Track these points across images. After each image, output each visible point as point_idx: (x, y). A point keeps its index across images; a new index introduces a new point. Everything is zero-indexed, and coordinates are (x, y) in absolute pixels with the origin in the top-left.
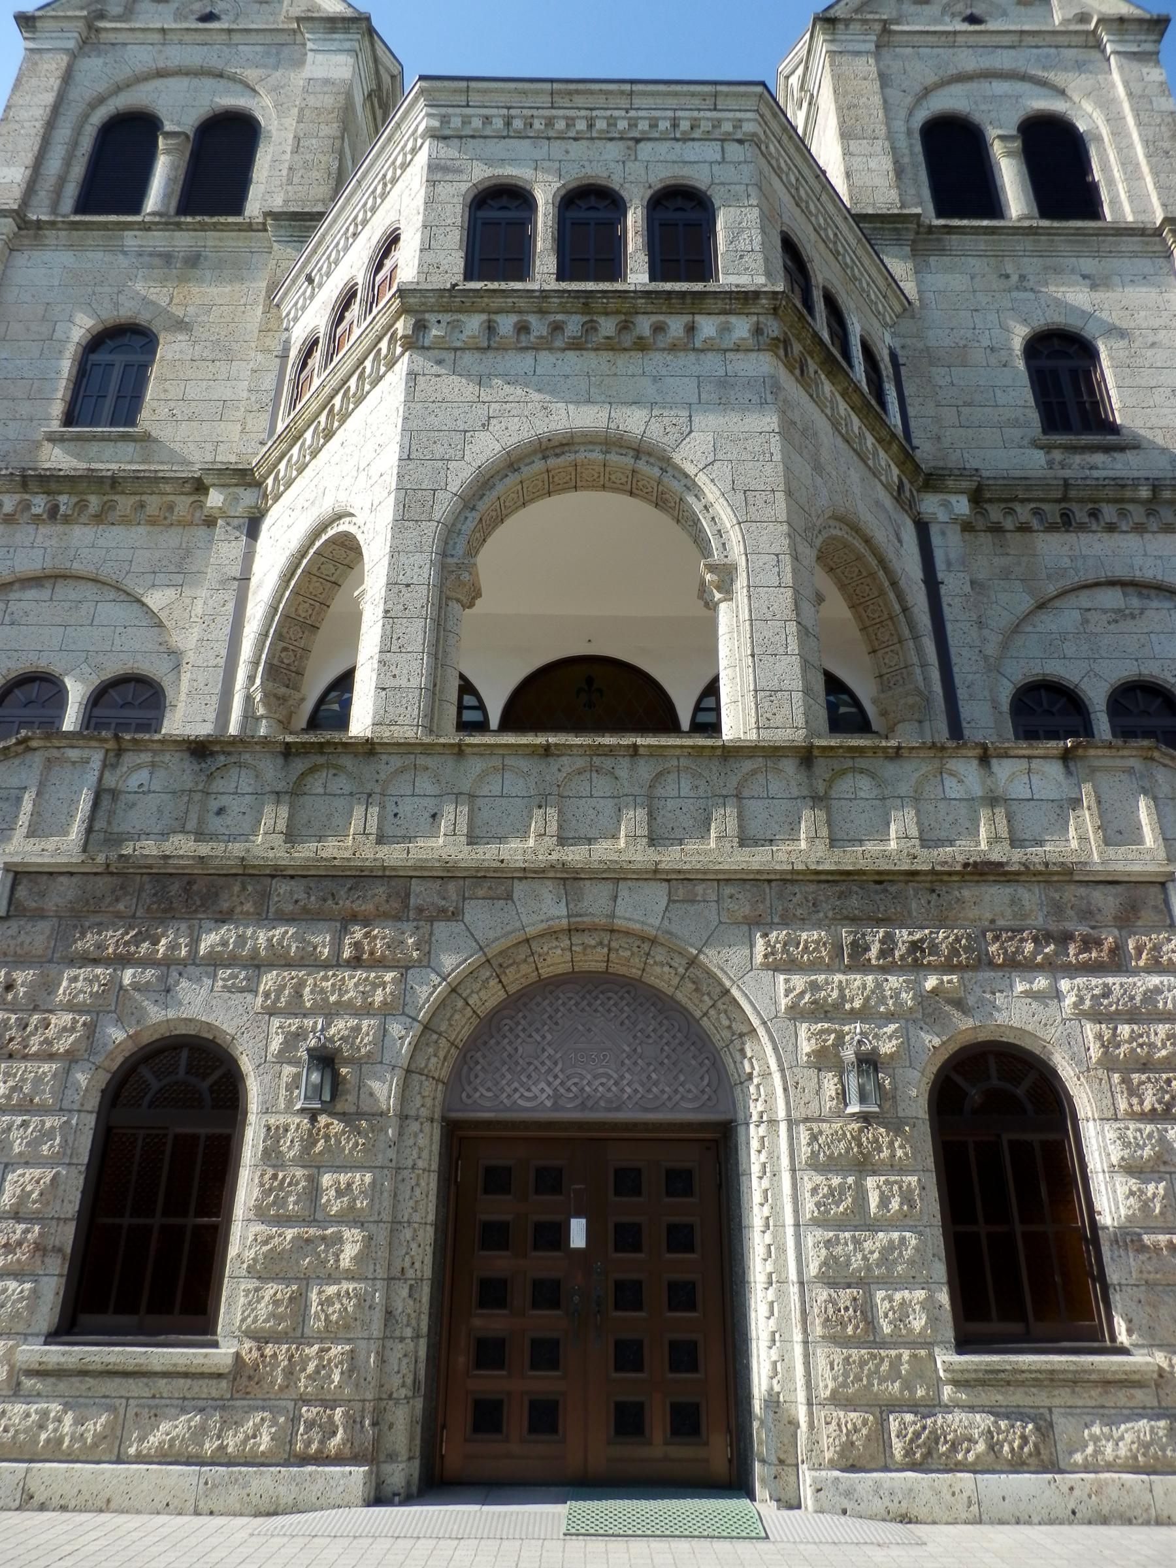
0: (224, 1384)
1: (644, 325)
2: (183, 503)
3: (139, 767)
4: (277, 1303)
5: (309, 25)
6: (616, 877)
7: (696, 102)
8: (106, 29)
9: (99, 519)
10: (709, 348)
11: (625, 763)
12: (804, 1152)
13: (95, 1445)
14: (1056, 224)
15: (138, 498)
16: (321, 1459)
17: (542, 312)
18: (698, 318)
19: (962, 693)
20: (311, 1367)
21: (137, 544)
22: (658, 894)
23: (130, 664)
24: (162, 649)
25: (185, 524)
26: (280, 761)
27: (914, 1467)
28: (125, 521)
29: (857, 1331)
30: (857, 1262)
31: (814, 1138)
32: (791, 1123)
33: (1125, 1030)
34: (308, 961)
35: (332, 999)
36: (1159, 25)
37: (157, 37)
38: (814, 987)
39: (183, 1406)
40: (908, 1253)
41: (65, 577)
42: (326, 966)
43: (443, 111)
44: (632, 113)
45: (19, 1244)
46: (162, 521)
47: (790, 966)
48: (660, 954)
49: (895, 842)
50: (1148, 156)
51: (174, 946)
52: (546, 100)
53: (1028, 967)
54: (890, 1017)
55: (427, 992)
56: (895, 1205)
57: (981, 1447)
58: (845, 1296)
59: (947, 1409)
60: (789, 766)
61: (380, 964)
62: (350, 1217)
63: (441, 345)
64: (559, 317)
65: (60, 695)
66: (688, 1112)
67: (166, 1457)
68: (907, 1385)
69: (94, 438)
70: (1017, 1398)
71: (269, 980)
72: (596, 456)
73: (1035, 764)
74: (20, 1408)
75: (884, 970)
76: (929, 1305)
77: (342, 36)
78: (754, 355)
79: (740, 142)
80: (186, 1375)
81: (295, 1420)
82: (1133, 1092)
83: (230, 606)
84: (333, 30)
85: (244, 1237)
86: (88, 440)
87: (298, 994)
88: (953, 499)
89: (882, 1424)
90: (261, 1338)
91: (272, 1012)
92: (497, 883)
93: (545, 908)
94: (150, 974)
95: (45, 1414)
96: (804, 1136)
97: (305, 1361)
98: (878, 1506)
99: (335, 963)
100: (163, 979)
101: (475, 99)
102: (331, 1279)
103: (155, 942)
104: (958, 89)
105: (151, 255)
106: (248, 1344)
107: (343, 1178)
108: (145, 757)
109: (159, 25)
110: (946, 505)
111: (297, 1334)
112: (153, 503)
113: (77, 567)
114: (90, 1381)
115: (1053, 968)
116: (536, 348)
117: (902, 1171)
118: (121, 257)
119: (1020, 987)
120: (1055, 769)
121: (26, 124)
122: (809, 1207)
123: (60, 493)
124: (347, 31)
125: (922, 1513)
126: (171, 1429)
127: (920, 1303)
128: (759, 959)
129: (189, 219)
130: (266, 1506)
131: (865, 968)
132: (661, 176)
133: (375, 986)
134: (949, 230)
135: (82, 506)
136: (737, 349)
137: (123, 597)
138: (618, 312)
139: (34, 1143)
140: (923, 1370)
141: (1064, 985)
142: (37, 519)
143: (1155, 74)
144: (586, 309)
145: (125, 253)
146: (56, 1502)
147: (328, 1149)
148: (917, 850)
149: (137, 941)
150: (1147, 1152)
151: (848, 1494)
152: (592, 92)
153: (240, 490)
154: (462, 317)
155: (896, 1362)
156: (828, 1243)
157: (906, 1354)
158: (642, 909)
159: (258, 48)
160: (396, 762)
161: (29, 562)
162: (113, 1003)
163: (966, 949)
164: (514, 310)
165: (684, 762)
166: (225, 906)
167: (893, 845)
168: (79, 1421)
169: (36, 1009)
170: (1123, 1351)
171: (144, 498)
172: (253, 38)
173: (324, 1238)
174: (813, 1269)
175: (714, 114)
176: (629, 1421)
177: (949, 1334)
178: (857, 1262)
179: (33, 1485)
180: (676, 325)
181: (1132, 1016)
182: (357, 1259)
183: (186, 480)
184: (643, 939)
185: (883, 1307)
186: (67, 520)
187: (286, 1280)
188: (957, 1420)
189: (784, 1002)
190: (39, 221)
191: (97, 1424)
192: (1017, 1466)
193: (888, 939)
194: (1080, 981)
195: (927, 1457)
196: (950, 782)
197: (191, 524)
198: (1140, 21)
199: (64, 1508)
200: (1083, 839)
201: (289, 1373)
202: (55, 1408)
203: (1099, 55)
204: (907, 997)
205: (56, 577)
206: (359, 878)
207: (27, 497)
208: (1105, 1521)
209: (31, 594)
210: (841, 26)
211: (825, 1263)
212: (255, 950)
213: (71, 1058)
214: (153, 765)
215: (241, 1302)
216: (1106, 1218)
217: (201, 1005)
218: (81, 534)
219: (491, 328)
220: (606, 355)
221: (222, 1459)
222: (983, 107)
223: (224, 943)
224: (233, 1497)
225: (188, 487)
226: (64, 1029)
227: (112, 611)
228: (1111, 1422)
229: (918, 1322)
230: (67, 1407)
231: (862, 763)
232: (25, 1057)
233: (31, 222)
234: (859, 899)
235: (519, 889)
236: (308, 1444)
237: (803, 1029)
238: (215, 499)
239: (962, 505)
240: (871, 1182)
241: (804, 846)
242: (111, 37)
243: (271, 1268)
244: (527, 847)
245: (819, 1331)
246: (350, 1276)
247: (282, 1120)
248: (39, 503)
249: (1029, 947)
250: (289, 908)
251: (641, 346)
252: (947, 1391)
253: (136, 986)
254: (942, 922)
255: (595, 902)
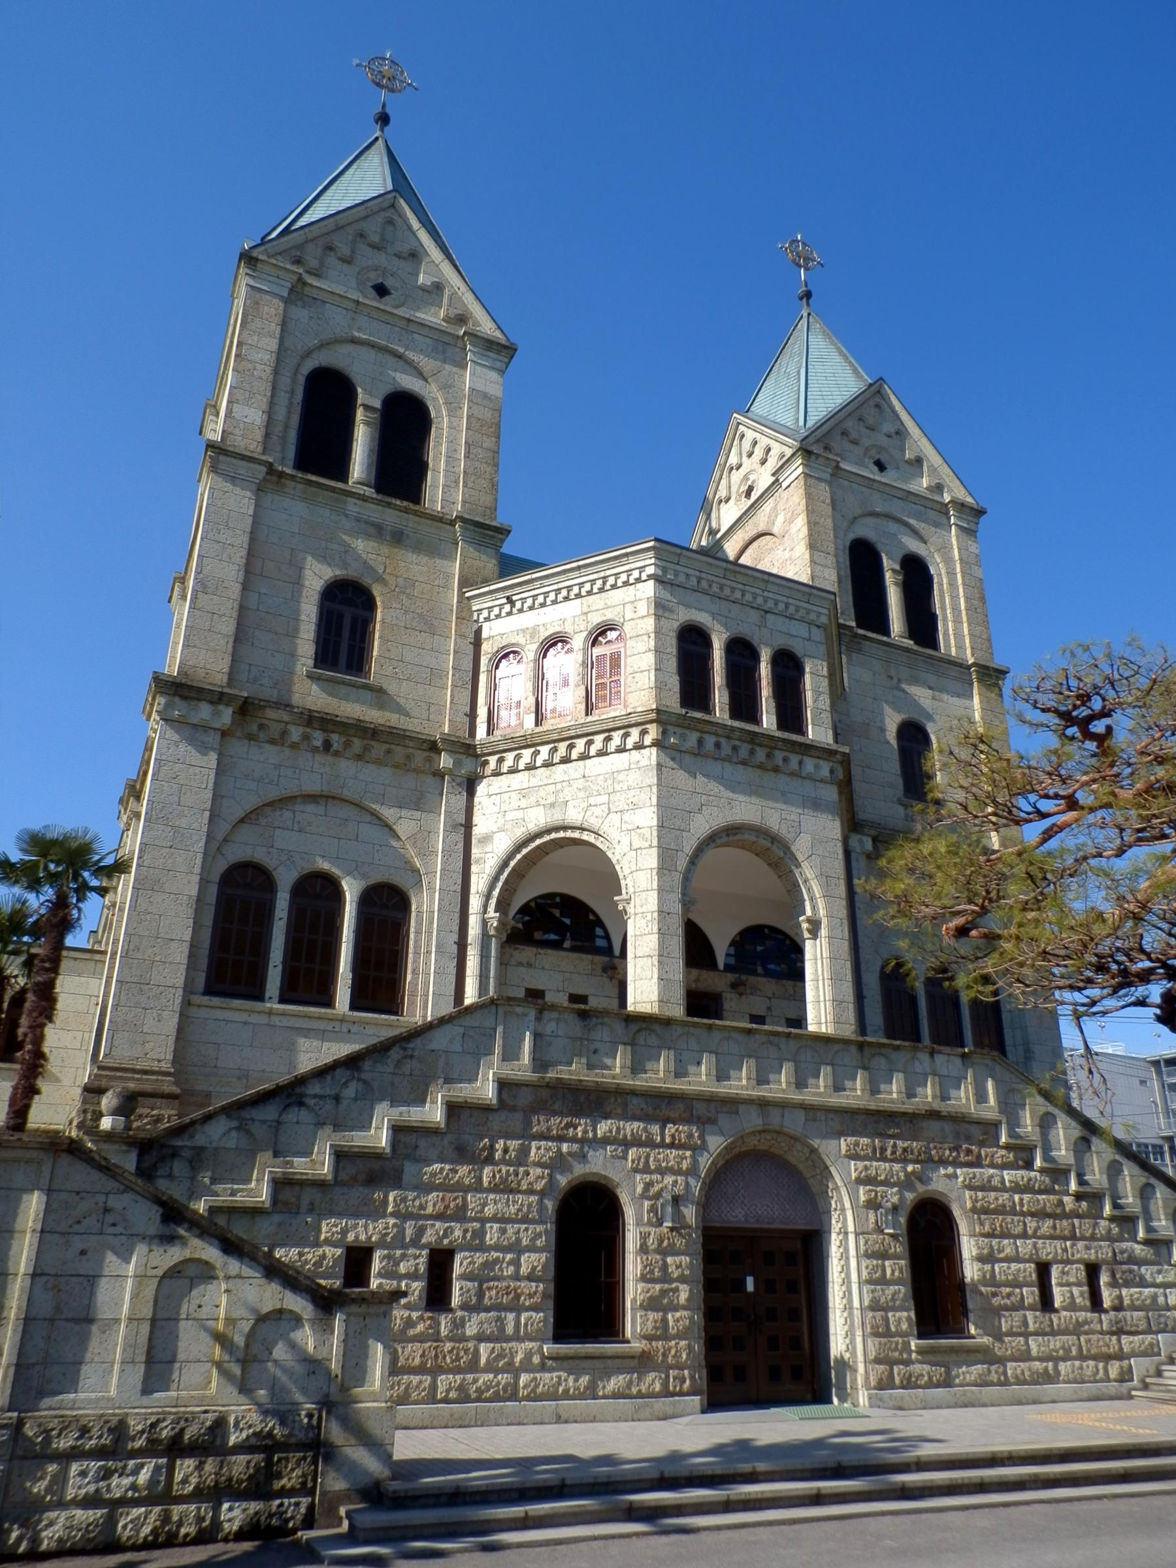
0: (636, 1361)
1: (779, 755)
2: (420, 757)
3: (551, 1020)
4: (656, 1322)
5: (473, 339)
6: (784, 1105)
7: (799, 595)
8: (311, 286)
9: (359, 757)
10: (809, 777)
11: (783, 1040)
12: (862, 1248)
13: (585, 1391)
14: (920, 649)
15: (388, 746)
16: (681, 1394)
17: (728, 737)
18: (805, 758)
19: (863, 966)
20: (673, 1352)
21: (387, 782)
22: (800, 1115)
23: (386, 876)
24: (408, 867)
25: (417, 771)
26: (623, 1024)
27: (903, 1388)
28: (378, 762)
29: (881, 1332)
30: (883, 1300)
31: (866, 1242)
32: (857, 1234)
33: (980, 1194)
34: (650, 1144)
35: (664, 1165)
36: (980, 512)
37: (351, 305)
38: (866, 1168)
39: (620, 1371)
40: (901, 1295)
41: (334, 798)
42: (658, 1146)
43: (664, 564)
44: (766, 594)
45: (535, 1293)
46: (402, 767)
47: (856, 1157)
48: (798, 1146)
49: (893, 1092)
50: (967, 610)
51: (585, 1132)
52: (721, 573)
53: (943, 1162)
54: (893, 1185)
55: (705, 1162)
56: (897, 1274)
57: (926, 1378)
58: (879, 1314)
59: (913, 1363)
60: (853, 1049)
61: (681, 1146)
62: (682, 1279)
63: (674, 748)
64: (737, 743)
65: (337, 896)
66: (801, 1225)
67: (616, 1396)
68: (901, 1354)
69: (343, 683)
70: (939, 1358)
71: (632, 1153)
72: (753, 838)
73: (952, 1058)
74: (547, 1375)
75: (892, 1161)
76: (908, 1319)
77: (495, 356)
78: (828, 786)
79: (818, 627)
80: (618, 1357)
81: (667, 1376)
82: (982, 1224)
83: (461, 846)
84: (489, 349)
85: (633, 1291)
86: (339, 683)
87: (647, 1162)
88: (865, 839)
89: (892, 1370)
90: (650, 1338)
91: (636, 1170)
92: (731, 1104)
93: (753, 1120)
94: (575, 1147)
95: (559, 1378)
96: (862, 1242)
97: (670, 1349)
98: (891, 1404)
99: (663, 1145)
100: (582, 1149)
101: (683, 561)
102: (676, 1309)
103: (576, 1128)
104: (870, 521)
105: (366, 523)
106: (644, 1342)
107: (678, 1259)
108: (555, 1015)
109: (354, 297)
110: (861, 841)
111: (665, 1337)
112: (399, 751)
113: (346, 793)
114: (577, 1362)
115: (956, 1164)
116: (723, 760)
117: (899, 1259)
118: (344, 518)
119: (942, 1171)
120: (958, 1061)
121: (258, 366)
122: (865, 1274)
123: (332, 732)
124: (498, 352)
125: (906, 1406)
126: (615, 1383)
127: (903, 1319)
128: (843, 1152)
129: (398, 502)
130: (661, 1415)
131: (883, 1159)
132: (781, 642)
133: (682, 1159)
134: (865, 638)
135: (347, 744)
136: (821, 781)
137: (376, 821)
138: (766, 746)
139: (533, 1240)
140: (907, 1345)
141: (959, 1171)
142: (315, 750)
143: (974, 548)
144: (752, 742)
145: (346, 516)
146: (572, 1419)
147: (669, 1244)
148: (905, 1100)
149: (567, 1126)
150: (985, 1251)
151: (881, 1400)
152: (746, 575)
153: (463, 757)
154: (686, 731)
155: (897, 1343)
156: (873, 1291)
157: (900, 1340)
158: (794, 1123)
159: (429, 341)
160: (680, 1030)
161: (312, 784)
162: (558, 1163)
163: (925, 1153)
164: (716, 735)
165: (809, 1043)
166: (608, 1110)
167: (895, 1095)
168: (576, 1380)
169: (520, 1165)
170: (974, 1337)
171: (393, 747)
172: (425, 331)
173: (671, 1290)
174: (866, 1303)
175: (809, 607)
176: (775, 1374)
177: (550, 1334)
178: (883, 1300)
179: (561, 1412)
180: (794, 759)
181: (982, 1188)
182: (688, 1300)
183: (425, 741)
184: (791, 1137)
185: (891, 1320)
186: (337, 754)
187: (657, 1310)
188: (917, 1368)
189: (854, 1175)
190: (282, 472)
191: (584, 1380)
192: (938, 1385)
193: (895, 1146)
194: (965, 1170)
195: (909, 1383)
196: (917, 1063)
197: (423, 772)
198: (972, 509)
199: (576, 1422)
200: (968, 1099)
201: (664, 1355)
202: (564, 1375)
203: (946, 521)
204: (902, 1175)
205: (328, 797)
206: (671, 1098)
207: (308, 730)
208: (966, 1406)
209: (310, 808)
210: (813, 457)
211: (871, 1301)
212: (625, 1136)
213: (542, 1194)
214: (558, 1019)
215: (634, 1323)
216: (968, 1280)
217: (599, 1164)
218: (346, 767)
219: (700, 742)
220: (758, 771)
221: (640, 1395)
222: (883, 540)
223: (611, 1131)
224: (647, 1413)
225: (425, 746)
226: (539, 1177)
227: (369, 831)
228: (968, 1366)
229: (905, 1326)
230: (570, 1374)
231: (883, 1051)
232: (519, 1192)
233: (277, 471)
234: (877, 1122)
235: (742, 1108)
236: (675, 1387)
237: (861, 1189)
238: (445, 761)
239: (869, 845)
240: (887, 1263)
241: (856, 1093)
242: (314, 294)
243: (651, 1304)
244: (741, 1083)
245: (869, 1330)
246: (684, 1308)
247: (647, 1229)
248: (318, 738)
249: (947, 1152)
250: (638, 1112)
251: (776, 770)
252: (914, 1356)
253: (570, 1154)
254: (915, 1138)
255: (775, 1119)
